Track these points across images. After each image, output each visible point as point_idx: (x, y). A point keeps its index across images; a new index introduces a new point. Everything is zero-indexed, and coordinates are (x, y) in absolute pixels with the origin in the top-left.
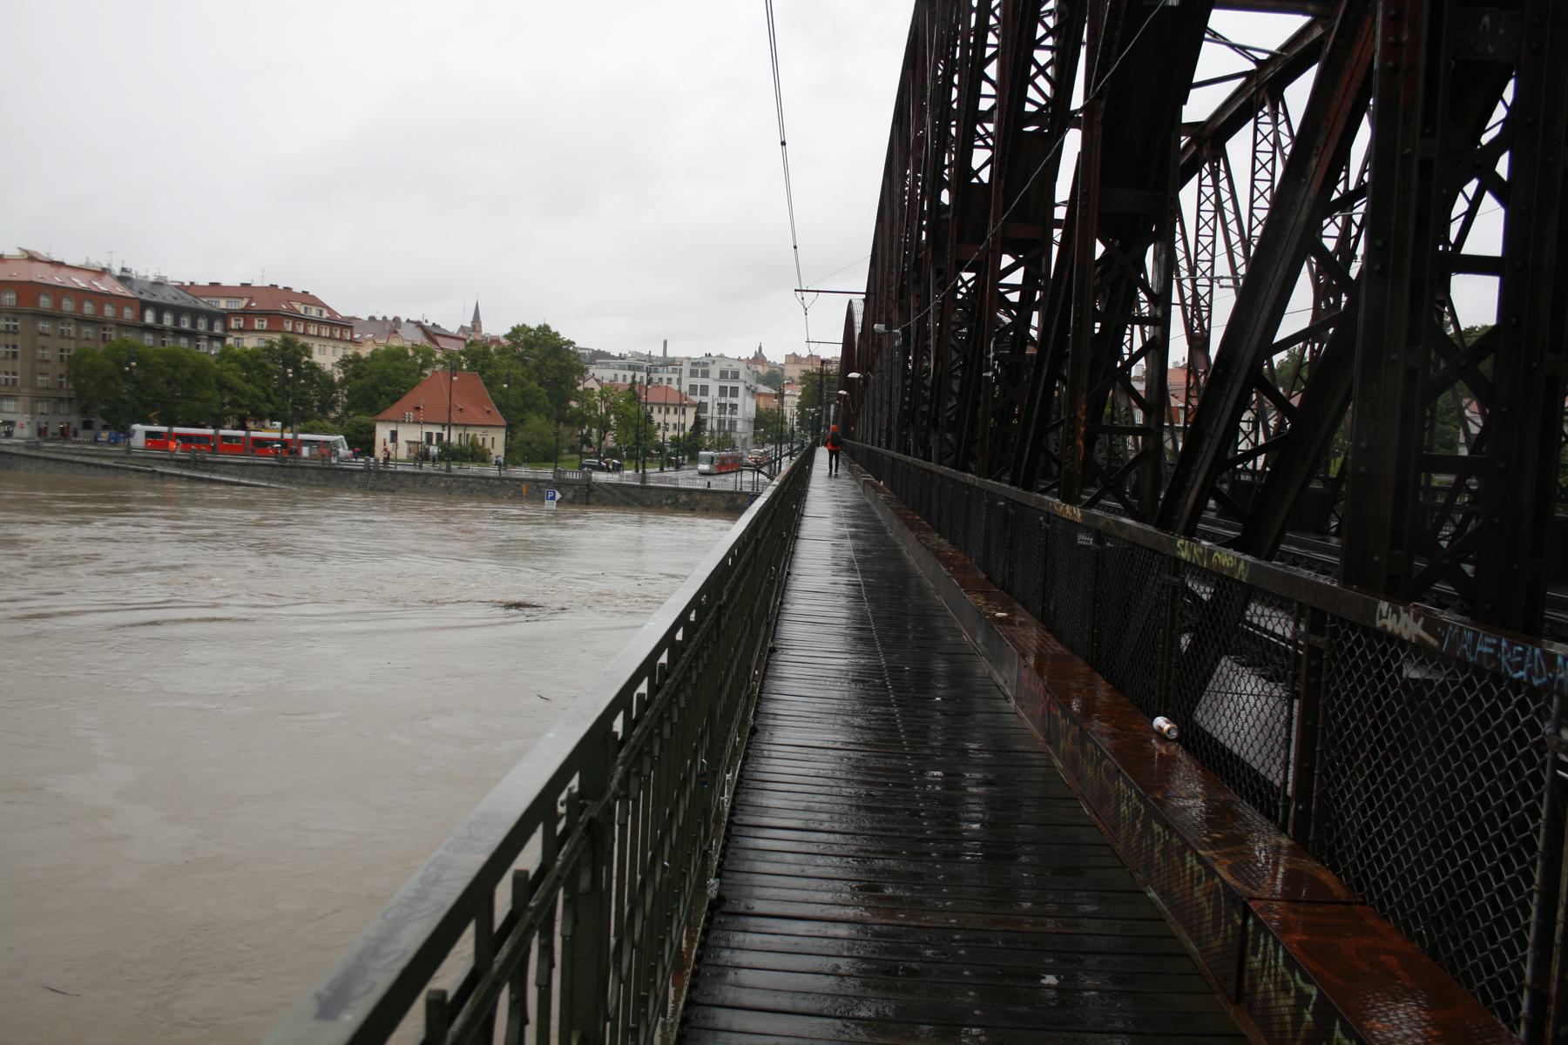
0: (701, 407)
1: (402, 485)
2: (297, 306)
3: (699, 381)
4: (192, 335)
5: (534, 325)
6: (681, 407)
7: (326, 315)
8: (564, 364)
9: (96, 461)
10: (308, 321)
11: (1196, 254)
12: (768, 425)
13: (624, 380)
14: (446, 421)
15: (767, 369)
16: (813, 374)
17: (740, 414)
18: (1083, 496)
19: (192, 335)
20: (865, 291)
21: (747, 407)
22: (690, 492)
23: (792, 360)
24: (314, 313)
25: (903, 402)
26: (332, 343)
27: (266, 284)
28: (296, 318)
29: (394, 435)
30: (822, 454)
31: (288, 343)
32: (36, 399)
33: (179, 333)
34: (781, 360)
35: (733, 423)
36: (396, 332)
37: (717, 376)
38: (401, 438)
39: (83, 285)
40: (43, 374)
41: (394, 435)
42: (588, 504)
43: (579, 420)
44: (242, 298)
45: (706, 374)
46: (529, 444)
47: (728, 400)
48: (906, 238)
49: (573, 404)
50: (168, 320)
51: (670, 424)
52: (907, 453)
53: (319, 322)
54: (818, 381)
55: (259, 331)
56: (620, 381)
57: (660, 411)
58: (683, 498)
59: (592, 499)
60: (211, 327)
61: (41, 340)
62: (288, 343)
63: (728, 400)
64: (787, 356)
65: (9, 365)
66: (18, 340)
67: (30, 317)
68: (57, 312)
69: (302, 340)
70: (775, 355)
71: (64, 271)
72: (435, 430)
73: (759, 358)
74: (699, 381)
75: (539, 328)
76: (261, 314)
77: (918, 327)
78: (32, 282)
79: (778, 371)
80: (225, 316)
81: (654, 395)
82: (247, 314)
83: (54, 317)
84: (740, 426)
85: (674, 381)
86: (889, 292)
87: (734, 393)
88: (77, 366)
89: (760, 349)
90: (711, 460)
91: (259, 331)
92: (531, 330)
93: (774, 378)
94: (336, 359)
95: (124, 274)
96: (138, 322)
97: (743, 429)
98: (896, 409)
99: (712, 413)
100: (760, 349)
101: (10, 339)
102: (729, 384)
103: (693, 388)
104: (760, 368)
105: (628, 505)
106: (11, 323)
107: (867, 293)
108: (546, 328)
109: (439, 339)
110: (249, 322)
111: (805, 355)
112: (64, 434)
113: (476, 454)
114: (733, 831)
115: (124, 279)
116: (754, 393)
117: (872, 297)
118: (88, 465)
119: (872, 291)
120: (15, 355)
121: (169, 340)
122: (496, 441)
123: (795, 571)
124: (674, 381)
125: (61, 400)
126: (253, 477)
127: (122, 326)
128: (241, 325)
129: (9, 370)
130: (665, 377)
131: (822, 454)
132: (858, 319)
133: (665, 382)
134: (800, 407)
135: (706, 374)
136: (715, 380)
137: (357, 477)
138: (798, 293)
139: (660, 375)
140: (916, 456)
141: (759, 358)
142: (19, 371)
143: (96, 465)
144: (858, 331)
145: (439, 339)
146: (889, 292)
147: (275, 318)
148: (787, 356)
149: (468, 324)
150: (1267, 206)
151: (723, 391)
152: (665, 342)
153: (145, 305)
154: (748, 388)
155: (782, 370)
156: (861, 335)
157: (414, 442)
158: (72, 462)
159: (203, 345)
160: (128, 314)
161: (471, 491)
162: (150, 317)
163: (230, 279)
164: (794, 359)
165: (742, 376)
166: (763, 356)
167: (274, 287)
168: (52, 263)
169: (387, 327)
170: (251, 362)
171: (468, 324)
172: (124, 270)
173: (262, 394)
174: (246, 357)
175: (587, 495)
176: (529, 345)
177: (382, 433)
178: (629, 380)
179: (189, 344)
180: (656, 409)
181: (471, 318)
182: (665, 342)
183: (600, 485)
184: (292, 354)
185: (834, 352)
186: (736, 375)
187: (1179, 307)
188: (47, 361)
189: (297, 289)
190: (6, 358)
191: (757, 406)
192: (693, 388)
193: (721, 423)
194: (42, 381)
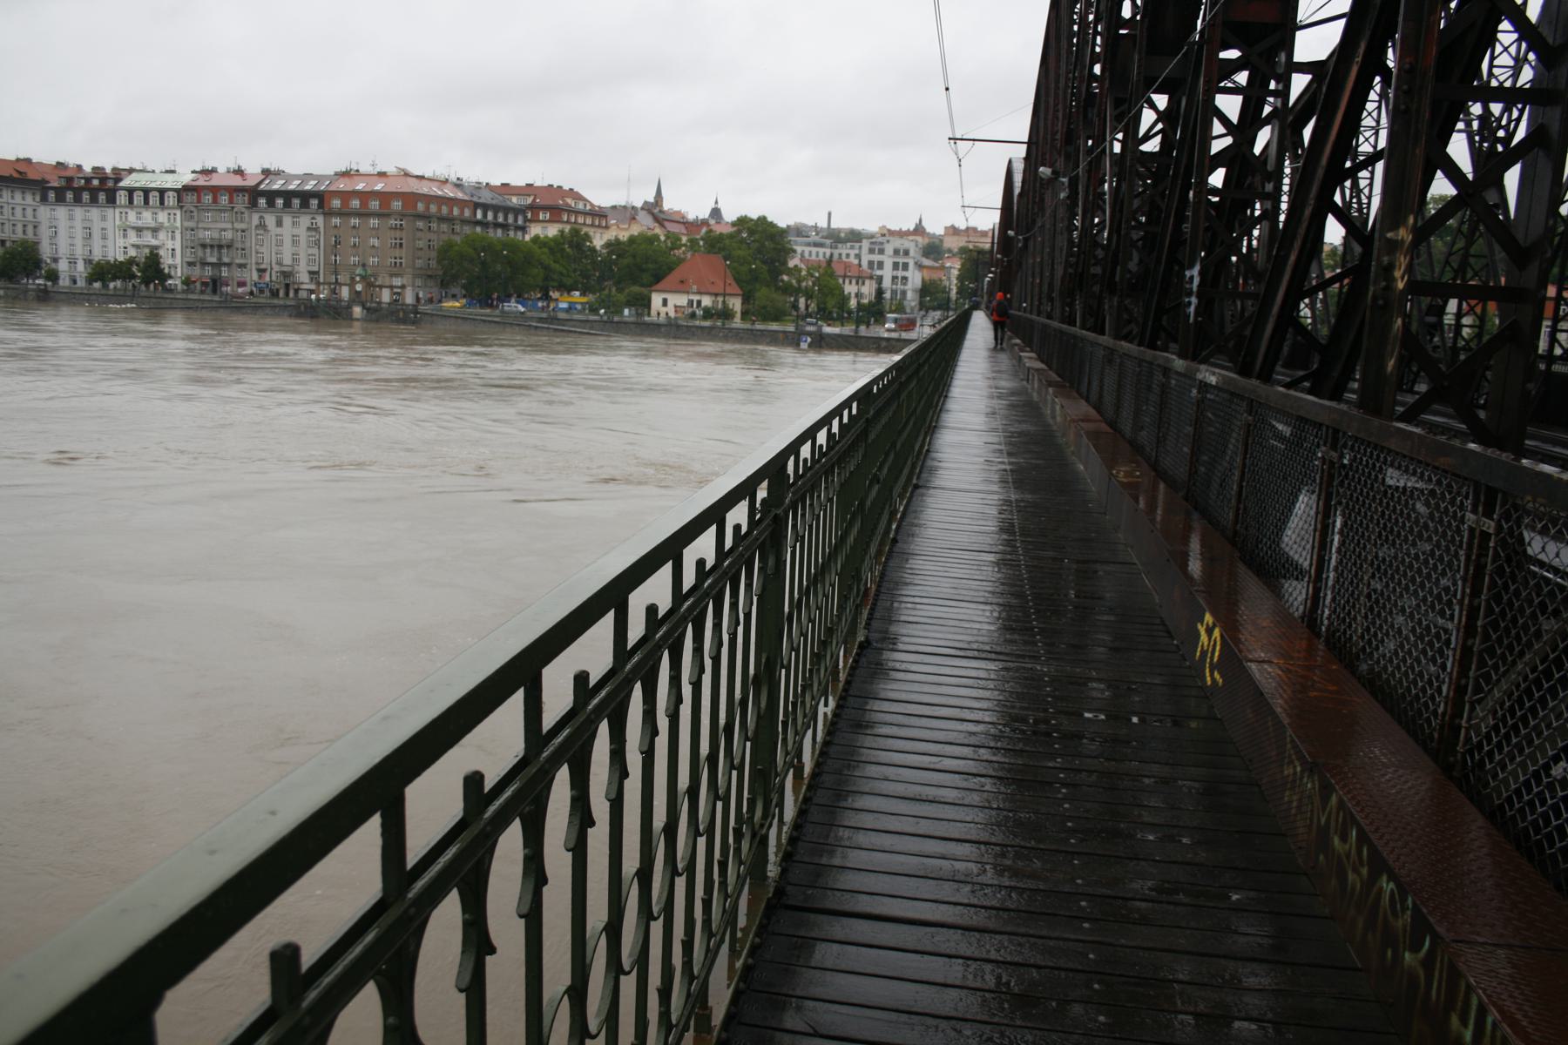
0: (880, 279)
1: (694, 335)
2: (569, 201)
3: (876, 258)
4: (505, 227)
5: (754, 216)
6: (860, 279)
7: (588, 207)
8: (779, 247)
9: (490, 319)
10: (577, 213)
11: (1379, 108)
12: (931, 294)
13: (824, 257)
14: (722, 291)
15: (927, 241)
16: (971, 251)
17: (909, 286)
18: (1397, 408)
19: (505, 227)
20: (1026, 140)
21: (915, 279)
22: (888, 340)
23: (951, 231)
24: (581, 206)
25: (1067, 264)
26: (600, 230)
27: (546, 185)
28: (571, 211)
29: (665, 302)
30: (980, 328)
31: (575, 232)
32: (415, 276)
33: (497, 225)
34: (940, 231)
35: (904, 293)
36: (634, 219)
37: (891, 253)
38: (671, 304)
39: (451, 195)
40: (418, 258)
41: (665, 302)
42: (821, 347)
43: (787, 290)
44: (529, 195)
45: (881, 252)
46: (764, 307)
47: (900, 273)
48: (1073, 88)
49: (785, 278)
50: (490, 216)
51: (857, 292)
52: (1072, 323)
53: (585, 214)
54: (975, 261)
55: (543, 221)
56: (821, 257)
57: (850, 282)
58: (884, 344)
59: (823, 344)
60: (516, 220)
61: (419, 234)
62: (575, 232)
63: (900, 273)
64: (946, 228)
65: (397, 253)
66: (404, 234)
67: (411, 218)
68: (427, 213)
69: (585, 230)
70: (935, 227)
71: (425, 182)
72: (695, 298)
73: (919, 230)
74: (876, 258)
75: (759, 218)
76: (544, 208)
77: (1089, 178)
78: (413, 193)
79: (937, 241)
80: (517, 211)
81: (839, 270)
82: (534, 208)
83: (425, 217)
84: (910, 295)
85: (852, 257)
86: (1054, 140)
87: (905, 267)
88: (445, 252)
89: (920, 221)
90: (895, 321)
91: (543, 221)
92: (752, 220)
93: (933, 249)
94: (603, 243)
95: (459, 182)
96: (474, 219)
97: (911, 299)
98: (1059, 272)
99: (887, 283)
100: (920, 221)
101: (398, 234)
102: (901, 260)
103: (871, 263)
104: (919, 239)
105: (847, 349)
106: (398, 222)
107: (1029, 143)
108: (764, 218)
109: (666, 224)
110: (535, 215)
111: (963, 227)
112: (431, 301)
113: (726, 314)
114: (950, 386)
115: (459, 185)
116: (920, 267)
117: (1034, 147)
118: (484, 321)
119: (1034, 140)
120: (401, 245)
121: (491, 231)
122: (736, 304)
123: (950, 395)
124: (852, 257)
125: (430, 277)
126: (591, 328)
127: (464, 222)
128: (548, 218)
129: (397, 255)
130: (844, 252)
131: (980, 328)
132: (1018, 179)
133: (844, 257)
134: (960, 278)
135: (881, 252)
136: (890, 256)
137: (663, 329)
138: (952, 142)
139: (841, 251)
140: (1083, 327)
141: (919, 230)
142: (404, 256)
143: (489, 321)
144: (1017, 191)
145: (666, 224)
146: (1054, 140)
147: (556, 212)
148: (946, 228)
149: (652, 200)
150: (1500, 36)
151: (896, 266)
152: (830, 214)
153: (477, 206)
154: (916, 263)
155: (941, 241)
156: (1020, 195)
157: (680, 307)
158: (474, 319)
159: (511, 233)
160: (467, 213)
161: (742, 338)
162: (479, 215)
163: (518, 181)
164: (953, 231)
165: (912, 253)
166: (923, 228)
167: (551, 186)
168: (417, 177)
169: (628, 215)
170: (554, 246)
171: (652, 200)
172: (458, 179)
173: (565, 271)
174: (552, 244)
175: (820, 341)
176: (751, 232)
177: (656, 299)
178: (828, 255)
179: (503, 233)
180: (847, 281)
181: (654, 194)
182: (830, 214)
183: (829, 335)
184: (577, 241)
185: (989, 220)
186: (906, 253)
187: (1464, 136)
188: (421, 249)
189: (566, 187)
190: (395, 247)
191: (923, 279)
192: (871, 263)
193: (894, 292)
194: (419, 263)
